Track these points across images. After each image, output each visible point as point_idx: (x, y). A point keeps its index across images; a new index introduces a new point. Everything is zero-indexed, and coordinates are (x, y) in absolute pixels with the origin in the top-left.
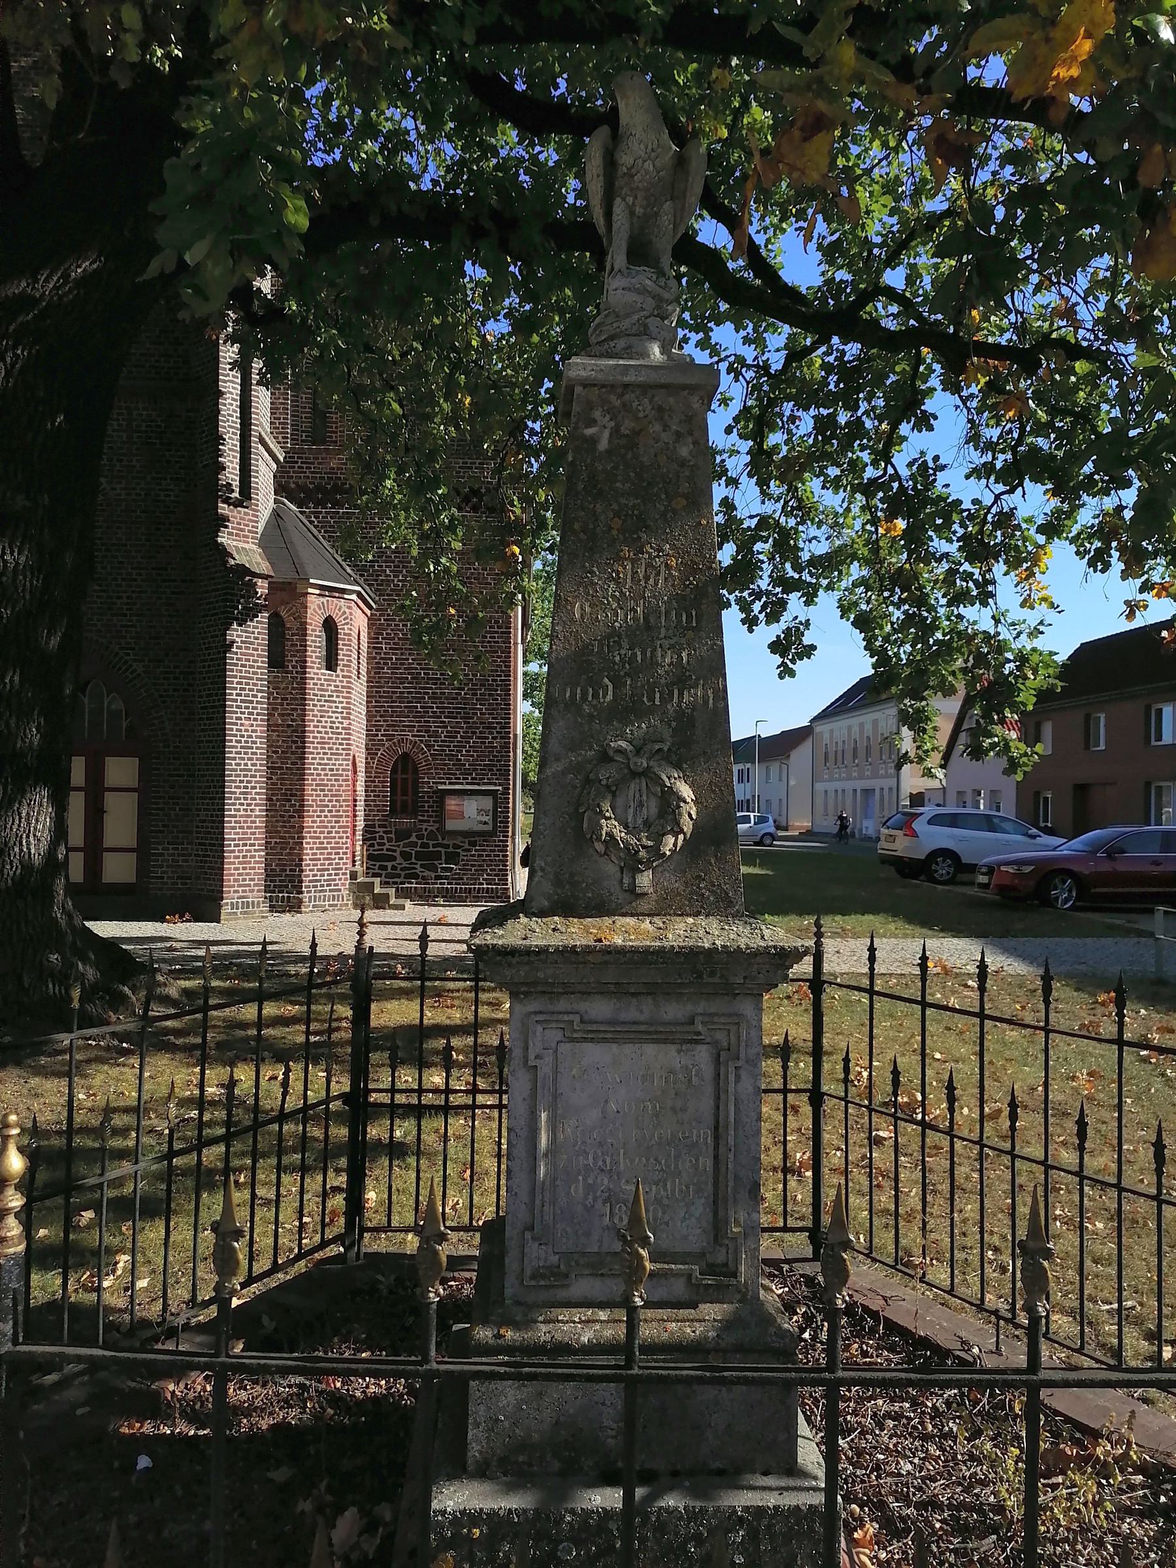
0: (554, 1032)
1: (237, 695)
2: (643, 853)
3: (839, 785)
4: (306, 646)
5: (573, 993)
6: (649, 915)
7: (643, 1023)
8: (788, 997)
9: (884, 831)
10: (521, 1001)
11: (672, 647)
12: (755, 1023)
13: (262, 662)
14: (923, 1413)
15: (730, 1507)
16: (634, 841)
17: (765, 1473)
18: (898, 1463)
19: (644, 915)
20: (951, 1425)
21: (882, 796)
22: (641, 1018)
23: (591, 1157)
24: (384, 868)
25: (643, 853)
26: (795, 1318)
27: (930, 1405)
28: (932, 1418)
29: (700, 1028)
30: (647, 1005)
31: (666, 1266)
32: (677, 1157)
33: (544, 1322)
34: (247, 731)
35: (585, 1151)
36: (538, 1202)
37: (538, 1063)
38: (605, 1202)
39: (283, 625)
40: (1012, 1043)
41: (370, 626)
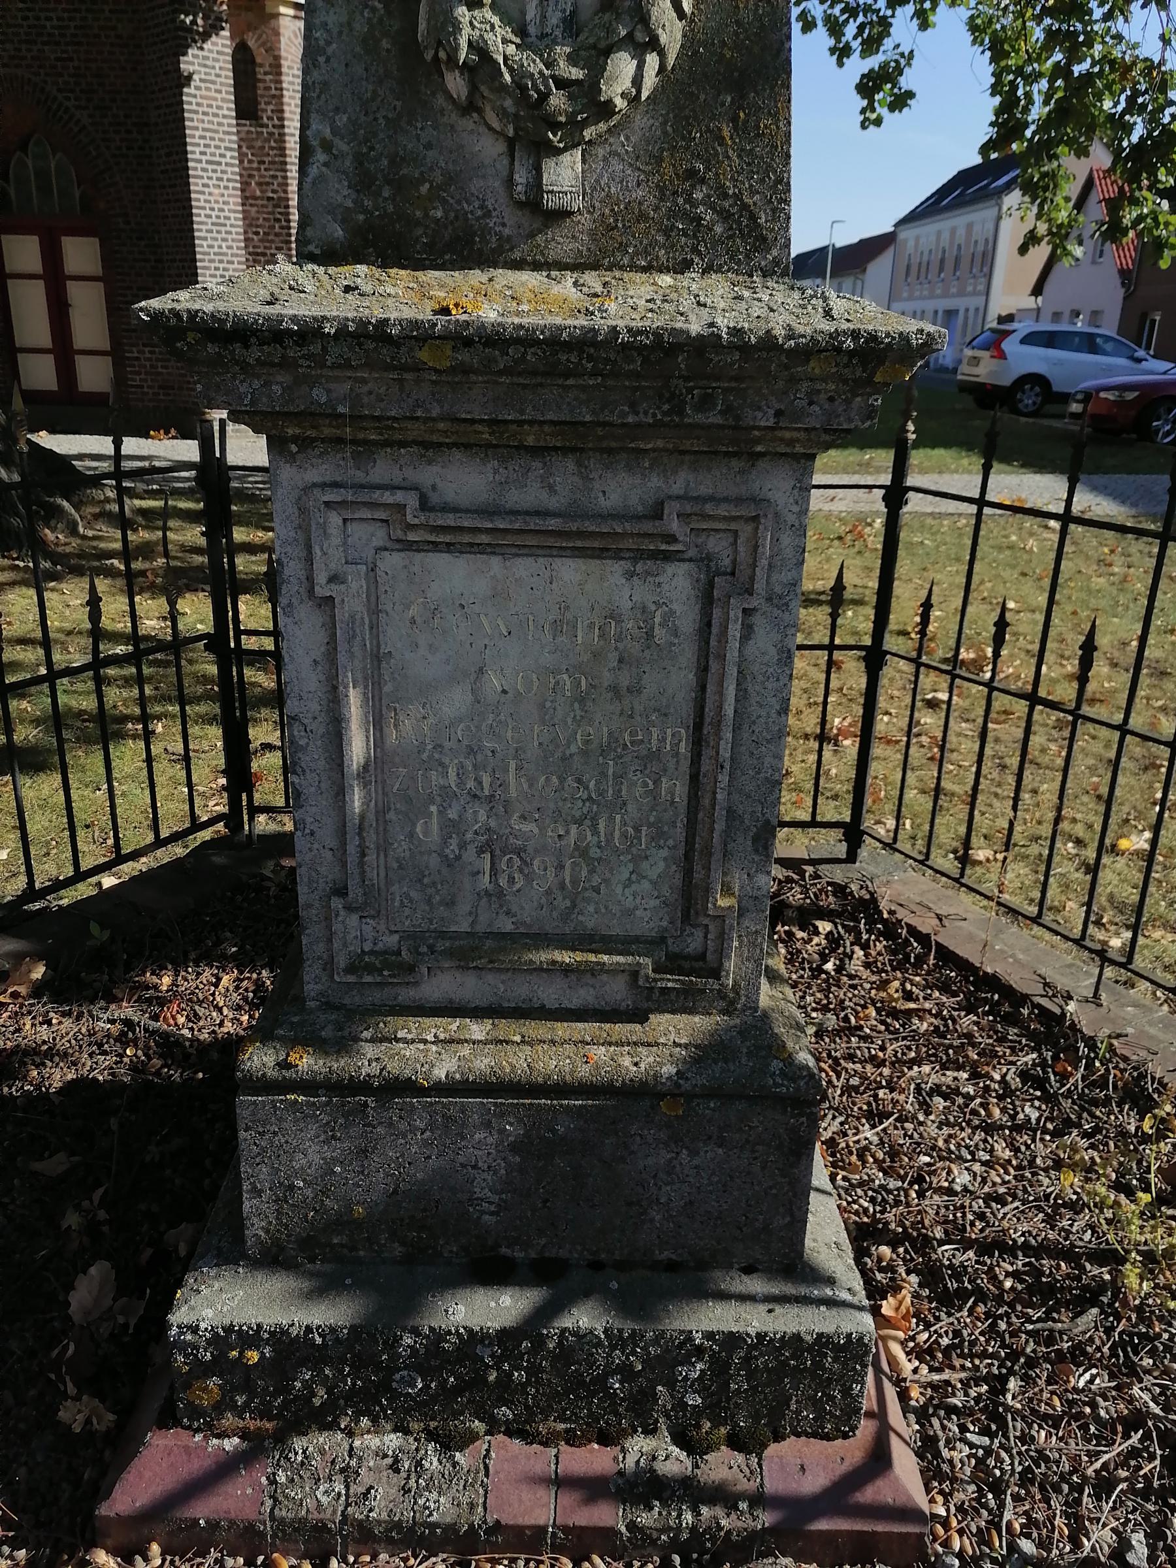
0: (370, 528)
1: (202, 153)
2: (558, 100)
4: (282, 89)
5: (403, 444)
6: (573, 268)
7: (554, 515)
8: (840, 538)
9: (969, 352)
10: (292, 458)
12: (791, 519)
13: (228, 108)
14: (987, 1089)
15: (682, 1332)
16: (536, 66)
17: (748, 1270)
18: (949, 1172)
19: (562, 267)
20: (1027, 1109)
21: (966, 318)
22: (553, 503)
23: (452, 773)
25: (558, 100)
26: (816, 940)
27: (997, 1077)
28: (1000, 1098)
29: (674, 525)
30: (565, 473)
31: (592, 958)
32: (619, 777)
33: (372, 1040)
34: (217, 202)
35: (441, 764)
36: (352, 849)
37: (333, 590)
38: (480, 851)
39: (253, 61)
40: (1099, 591)
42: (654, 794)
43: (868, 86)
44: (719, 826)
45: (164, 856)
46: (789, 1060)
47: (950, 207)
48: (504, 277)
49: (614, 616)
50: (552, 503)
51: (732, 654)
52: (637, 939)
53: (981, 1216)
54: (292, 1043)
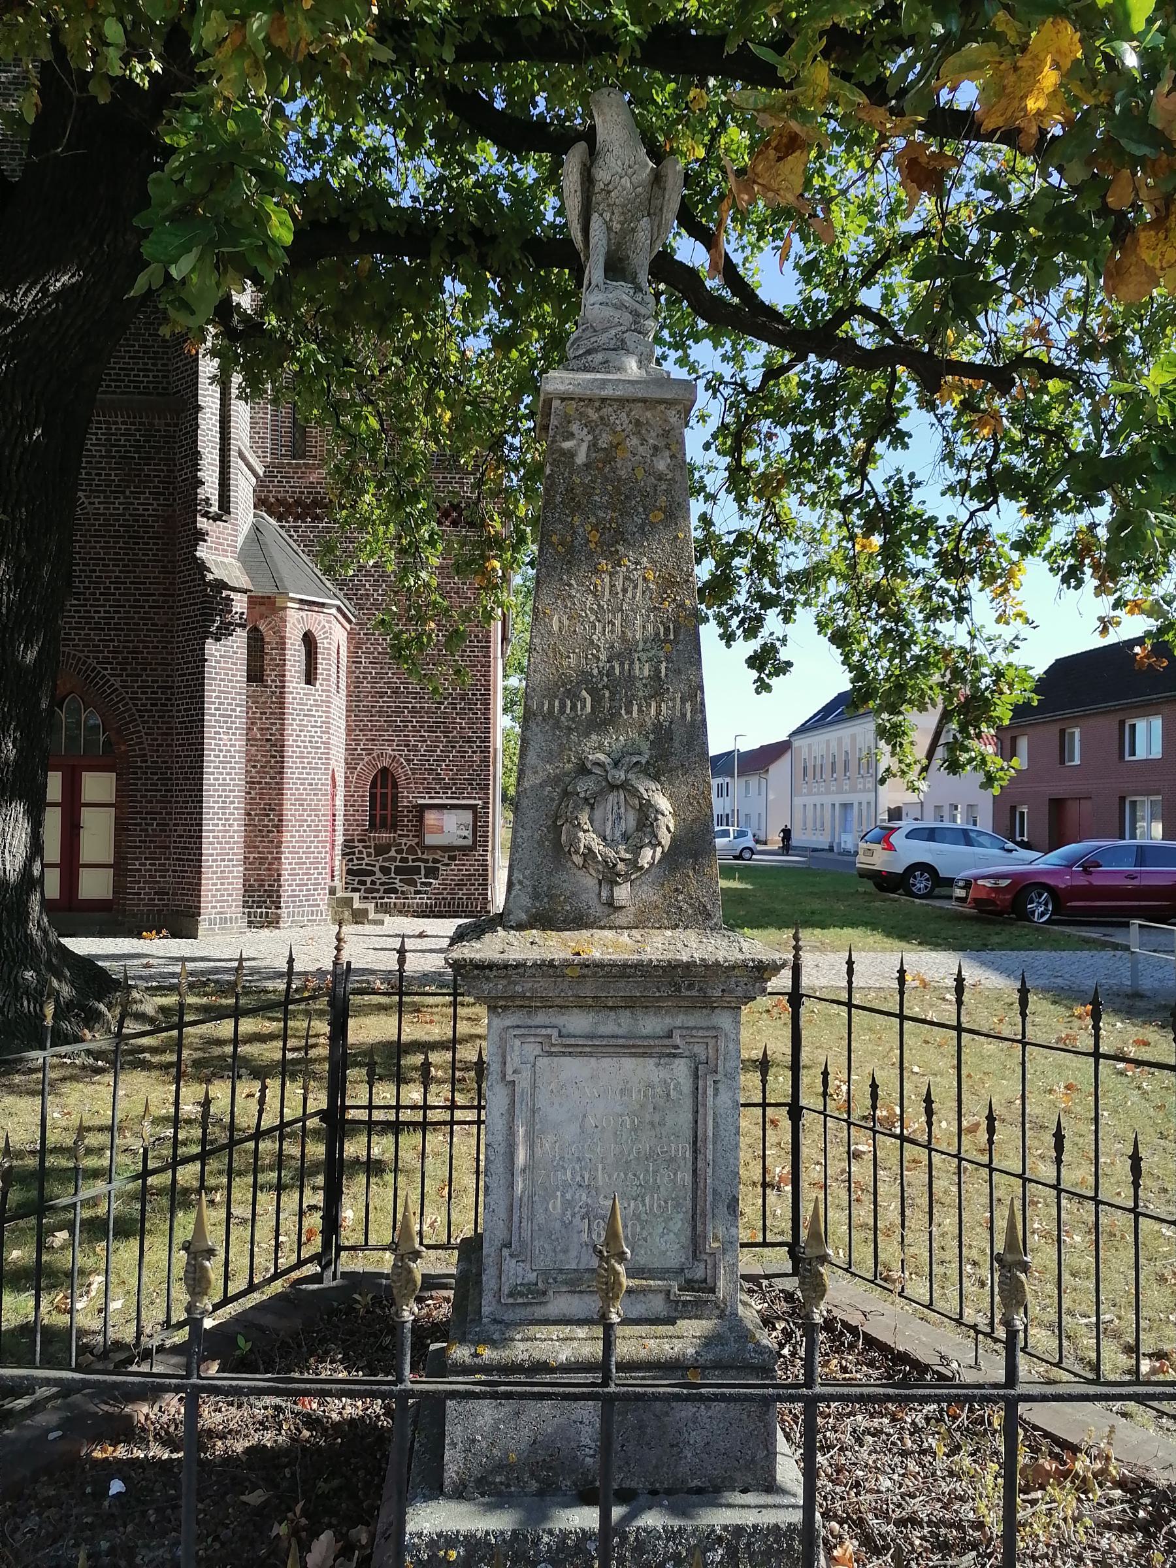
0: (532, 1046)
2: (621, 866)
3: (817, 800)
9: (862, 845)
11: (650, 660)
13: (242, 676)
14: (902, 1428)
16: (612, 854)
22: (620, 1032)
24: (364, 883)
25: (621, 866)
28: (911, 1434)
29: (678, 1041)
30: (625, 1018)
31: (644, 1282)
32: (655, 1172)
36: (515, 1219)
39: (262, 640)
41: (350, 640)
42: (674, 1181)
43: (757, 661)
44: (709, 1198)
45: (257, 1297)
46: (758, 1343)
47: (832, 723)
48: (599, 934)
49: (651, 1086)
50: (620, 1031)
51: (710, 1103)
52: (667, 1271)
53: (899, 1506)
54: (477, 1343)
